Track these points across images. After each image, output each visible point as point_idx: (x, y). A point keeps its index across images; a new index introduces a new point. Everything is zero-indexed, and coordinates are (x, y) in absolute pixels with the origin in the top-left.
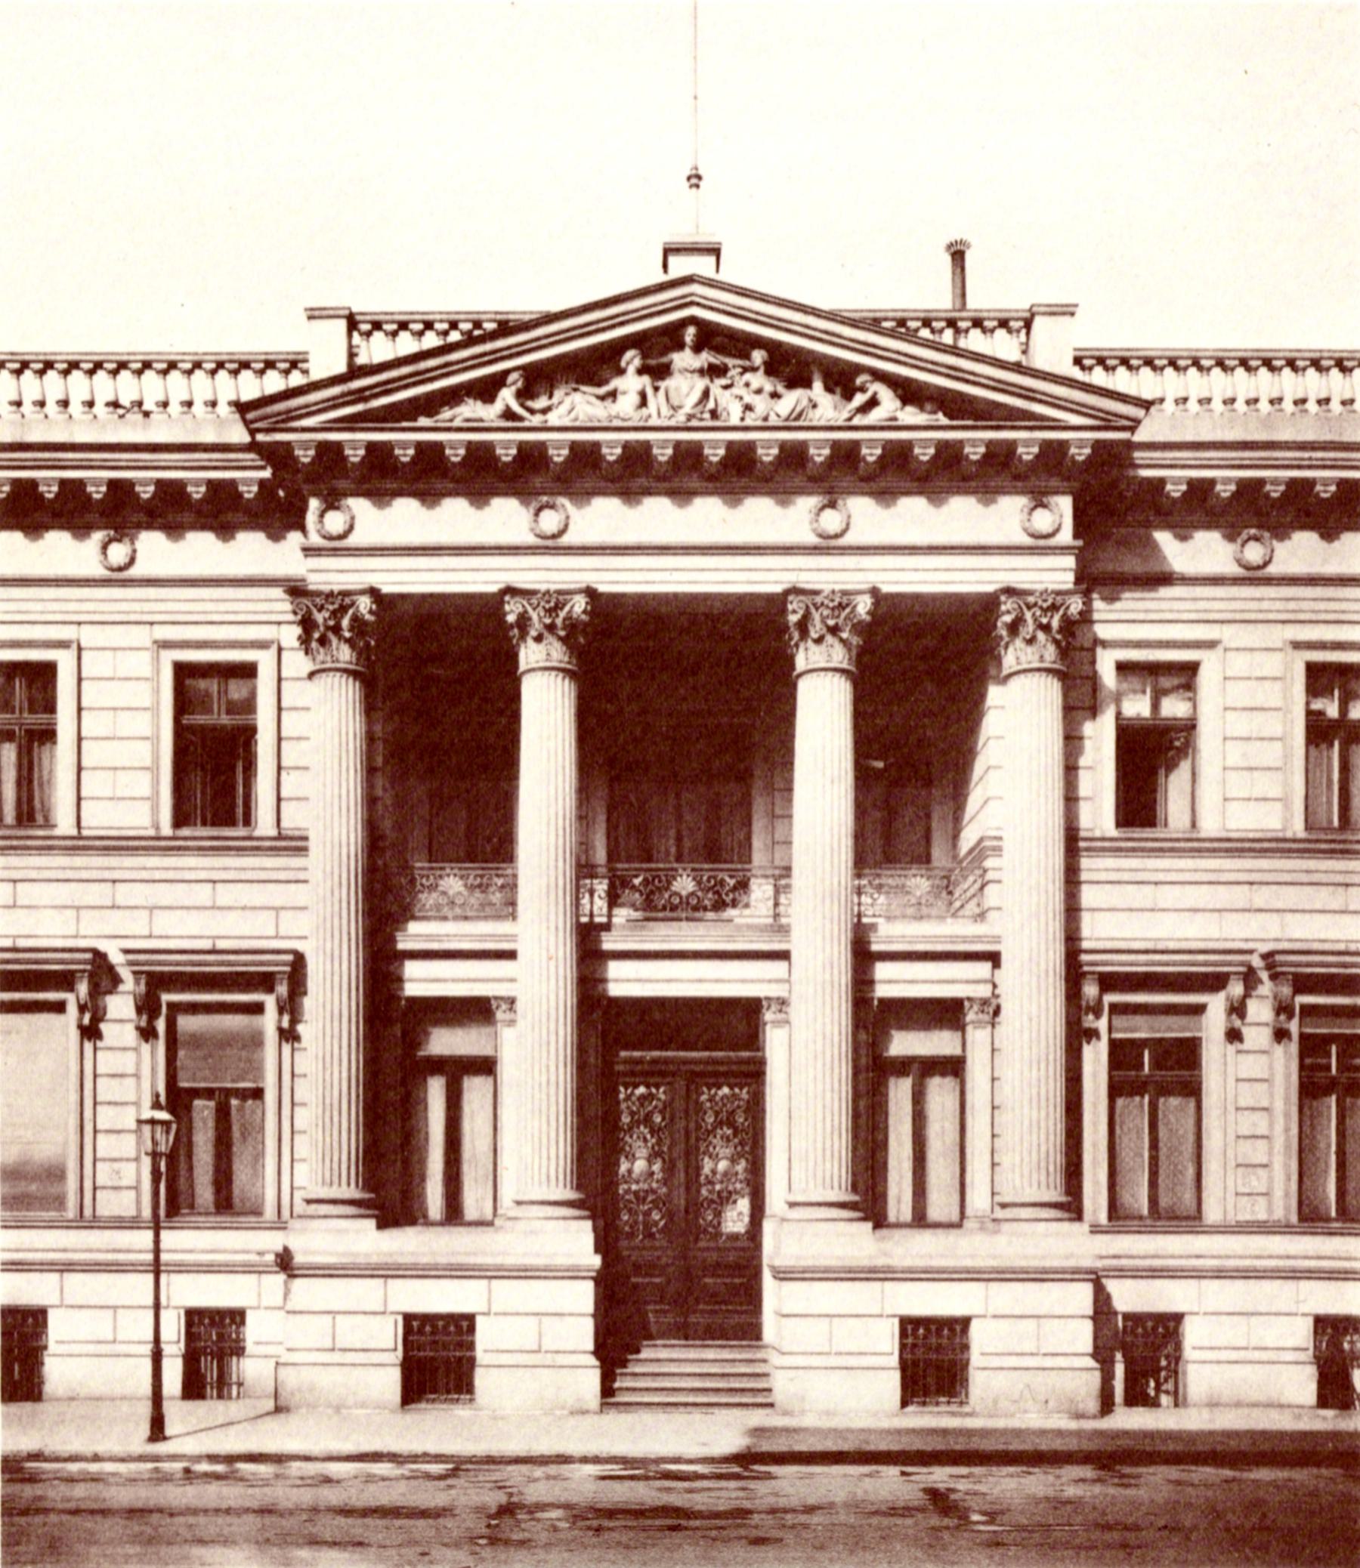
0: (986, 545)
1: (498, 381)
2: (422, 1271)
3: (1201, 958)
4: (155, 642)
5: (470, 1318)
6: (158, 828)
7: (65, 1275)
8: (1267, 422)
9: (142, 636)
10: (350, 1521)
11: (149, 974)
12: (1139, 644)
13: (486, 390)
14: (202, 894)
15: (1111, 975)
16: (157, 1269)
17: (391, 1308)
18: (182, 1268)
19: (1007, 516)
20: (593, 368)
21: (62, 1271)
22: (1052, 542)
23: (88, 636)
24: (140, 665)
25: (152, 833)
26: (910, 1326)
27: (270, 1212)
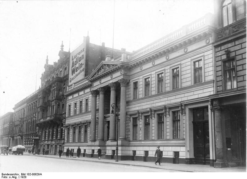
1: (96, 72)
13: (95, 74)
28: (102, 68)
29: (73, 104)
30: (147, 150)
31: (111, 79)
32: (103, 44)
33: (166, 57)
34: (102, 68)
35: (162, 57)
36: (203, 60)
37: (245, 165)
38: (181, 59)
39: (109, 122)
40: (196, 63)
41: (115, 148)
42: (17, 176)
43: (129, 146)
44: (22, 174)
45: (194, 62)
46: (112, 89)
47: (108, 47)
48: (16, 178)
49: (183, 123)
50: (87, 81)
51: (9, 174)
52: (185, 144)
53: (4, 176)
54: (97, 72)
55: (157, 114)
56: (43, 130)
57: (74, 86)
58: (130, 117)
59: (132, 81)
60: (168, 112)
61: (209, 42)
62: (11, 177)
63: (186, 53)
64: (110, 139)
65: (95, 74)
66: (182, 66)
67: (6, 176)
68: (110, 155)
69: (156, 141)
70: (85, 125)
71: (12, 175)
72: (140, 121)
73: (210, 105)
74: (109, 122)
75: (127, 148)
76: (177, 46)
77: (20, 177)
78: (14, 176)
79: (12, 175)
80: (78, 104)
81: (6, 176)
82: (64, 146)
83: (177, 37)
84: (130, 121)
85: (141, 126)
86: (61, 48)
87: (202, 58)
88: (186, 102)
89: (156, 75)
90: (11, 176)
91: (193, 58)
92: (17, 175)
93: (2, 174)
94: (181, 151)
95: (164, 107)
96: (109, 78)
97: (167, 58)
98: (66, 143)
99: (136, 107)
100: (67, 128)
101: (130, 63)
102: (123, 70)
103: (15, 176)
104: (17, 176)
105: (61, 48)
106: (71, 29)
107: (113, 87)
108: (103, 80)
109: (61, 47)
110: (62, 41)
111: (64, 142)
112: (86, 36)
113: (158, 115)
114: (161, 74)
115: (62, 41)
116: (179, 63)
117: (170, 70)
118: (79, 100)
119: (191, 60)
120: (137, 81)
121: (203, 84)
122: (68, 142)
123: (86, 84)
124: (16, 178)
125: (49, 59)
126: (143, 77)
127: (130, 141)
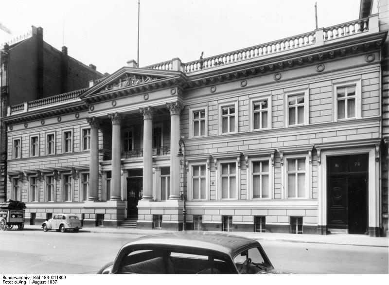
0: (165, 98)
1: (105, 86)
19: (167, 93)
20: (116, 82)
28: (120, 80)
31: (143, 100)
32: (65, 49)
33: (145, 96)
34: (120, 80)
37: (388, 213)
42: (27, 281)
44: (34, 277)
47: (73, 57)
48: (25, 284)
50: (80, 100)
51: (14, 278)
53: (7, 280)
54: (108, 86)
55: (192, 166)
62: (18, 282)
64: (172, 197)
65: (103, 88)
67: (9, 280)
68: (175, 224)
71: (19, 278)
77: (31, 282)
78: (22, 280)
79: (19, 278)
81: (9, 280)
83: (239, 60)
89: (63, 133)
90: (18, 281)
92: (26, 278)
93: (4, 277)
96: (108, 104)
101: (191, 78)
103: (23, 280)
104: (27, 281)
107: (95, 124)
119: (13, 138)
120: (36, 136)
123: (72, 105)
124: (25, 284)
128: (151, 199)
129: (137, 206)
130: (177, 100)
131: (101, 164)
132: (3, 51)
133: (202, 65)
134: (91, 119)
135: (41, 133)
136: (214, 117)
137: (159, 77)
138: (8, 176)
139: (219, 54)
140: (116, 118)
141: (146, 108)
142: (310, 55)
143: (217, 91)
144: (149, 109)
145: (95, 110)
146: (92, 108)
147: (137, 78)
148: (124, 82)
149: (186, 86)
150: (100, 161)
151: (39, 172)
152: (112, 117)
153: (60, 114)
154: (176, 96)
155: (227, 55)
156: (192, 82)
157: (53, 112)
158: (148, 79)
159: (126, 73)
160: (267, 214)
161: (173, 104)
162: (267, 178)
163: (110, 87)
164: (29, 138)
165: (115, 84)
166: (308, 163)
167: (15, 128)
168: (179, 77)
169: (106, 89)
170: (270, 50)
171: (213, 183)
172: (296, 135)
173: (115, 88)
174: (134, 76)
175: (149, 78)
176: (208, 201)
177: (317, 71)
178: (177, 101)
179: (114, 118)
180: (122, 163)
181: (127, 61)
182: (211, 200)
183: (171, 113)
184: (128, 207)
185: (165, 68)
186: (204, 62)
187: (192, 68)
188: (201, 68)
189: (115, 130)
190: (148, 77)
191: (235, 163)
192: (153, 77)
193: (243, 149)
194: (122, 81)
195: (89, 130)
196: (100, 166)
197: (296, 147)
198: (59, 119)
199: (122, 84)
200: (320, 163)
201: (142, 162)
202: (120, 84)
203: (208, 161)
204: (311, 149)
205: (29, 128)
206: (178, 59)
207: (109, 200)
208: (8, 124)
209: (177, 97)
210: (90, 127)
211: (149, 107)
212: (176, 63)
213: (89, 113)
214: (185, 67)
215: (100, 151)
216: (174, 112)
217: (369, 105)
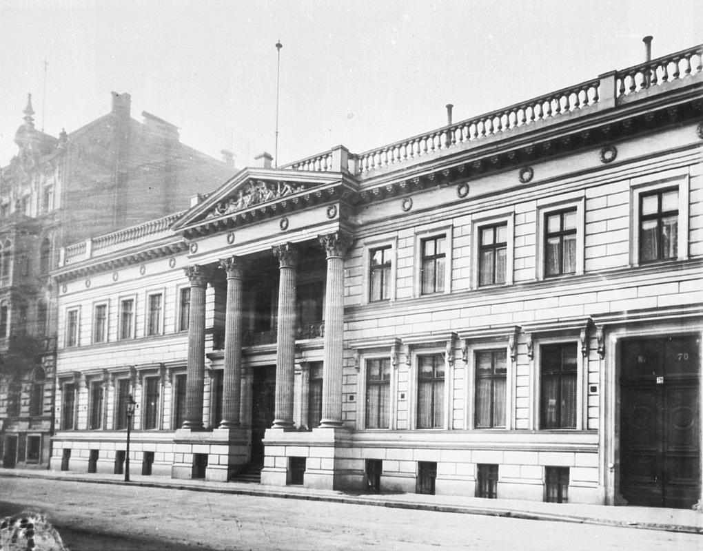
0: (315, 224)
1: (215, 206)
2: (556, 448)
3: (535, 327)
4: (631, 187)
5: (305, 458)
6: (472, 288)
7: (287, 447)
8: (482, 140)
9: (626, 185)
10: (89, 502)
11: (466, 340)
12: (549, 205)
13: (211, 210)
14: (486, 310)
15: (413, 345)
16: (128, 441)
17: (415, 459)
18: (134, 442)
19: (320, 215)
20: (233, 198)
21: (286, 446)
22: (287, 230)
23: (82, 303)
24: (411, 241)
25: (535, 280)
26: (549, 470)
27: (390, 428)
28: (241, 194)
29: (174, 291)
30: (151, 450)
33: (404, 203)
35: (180, 255)
36: (394, 247)
38: (508, 199)
39: (314, 367)
40: (427, 243)
41: (123, 447)
43: (352, 446)
45: (424, 241)
46: (229, 275)
49: (454, 389)
52: (598, 444)
54: (220, 205)
56: (18, 379)
57: (92, 250)
58: (359, 357)
59: (366, 244)
60: (407, 357)
61: (466, 194)
63: (408, 212)
64: (276, 423)
66: (590, 205)
69: (410, 431)
70: (68, 382)
72: (137, 388)
73: (583, 343)
74: (314, 367)
75: (349, 452)
76: (373, 194)
80: (115, 311)
82: (52, 441)
84: (358, 369)
85: (403, 387)
86: (25, 118)
87: (448, 232)
88: (537, 329)
89: (148, 297)
91: (544, 203)
94: (388, 458)
95: (396, 342)
97: (407, 205)
98: (60, 431)
99: (377, 328)
100: (117, 379)
102: (338, 206)
105: (25, 118)
106: (46, 63)
108: (295, 221)
109: (25, 115)
110: (30, 95)
111: (53, 426)
112: (61, 131)
113: (149, 379)
114: (382, 249)
115: (30, 95)
116: (510, 209)
117: (632, 194)
118: (118, 295)
120: (103, 303)
121: (676, 264)
122: (68, 424)
125: (34, 110)
126: (417, 234)
127: (353, 430)
128: (288, 426)
129: (263, 440)
130: (338, 229)
131: (209, 356)
132: (115, 115)
133: (449, 137)
134: (191, 269)
135: (167, 285)
136: (404, 258)
137: (308, 186)
138: (57, 380)
139: (478, 115)
140: (234, 266)
141: (283, 247)
142: (461, 163)
143: (534, 180)
144: (287, 247)
145: (199, 252)
146: (194, 248)
147: (269, 187)
148: (246, 197)
149: (351, 198)
150: (208, 351)
151: (133, 370)
152: (227, 265)
153: (143, 260)
154: (337, 220)
155: (435, 135)
156: (367, 191)
157: (133, 257)
158: (287, 189)
159: (251, 179)
160: (439, 460)
161: (331, 236)
162: (442, 384)
163: (223, 207)
164: (415, 241)
165: (232, 200)
166: (448, 363)
167: (72, 287)
168: (340, 184)
169: (217, 212)
170: (674, 71)
171: (403, 396)
172: (637, 287)
173: (231, 208)
174: (264, 185)
175: (289, 187)
176: (582, 432)
177: (520, 181)
178: (338, 232)
179: (229, 267)
180: (299, 349)
181: (254, 156)
182: (453, 429)
183: (328, 256)
184: (252, 442)
185: (314, 168)
186: (454, 131)
187: (429, 147)
188: (448, 144)
189: (232, 286)
190: (286, 186)
191: (506, 349)
192: (295, 185)
193: (400, 332)
194: (245, 194)
195: (189, 289)
196: (207, 360)
197: (491, 329)
198: (143, 270)
199: (243, 201)
200: (466, 361)
201: (275, 354)
202: (240, 200)
203: (583, 335)
204: (512, 332)
205: (93, 289)
206: (343, 148)
207: (180, 428)
208: (60, 282)
209: (338, 224)
210: (189, 285)
211: (288, 243)
212: (337, 158)
213: (189, 257)
214: (360, 161)
215: (209, 331)
216: (333, 253)
217: (605, 246)
